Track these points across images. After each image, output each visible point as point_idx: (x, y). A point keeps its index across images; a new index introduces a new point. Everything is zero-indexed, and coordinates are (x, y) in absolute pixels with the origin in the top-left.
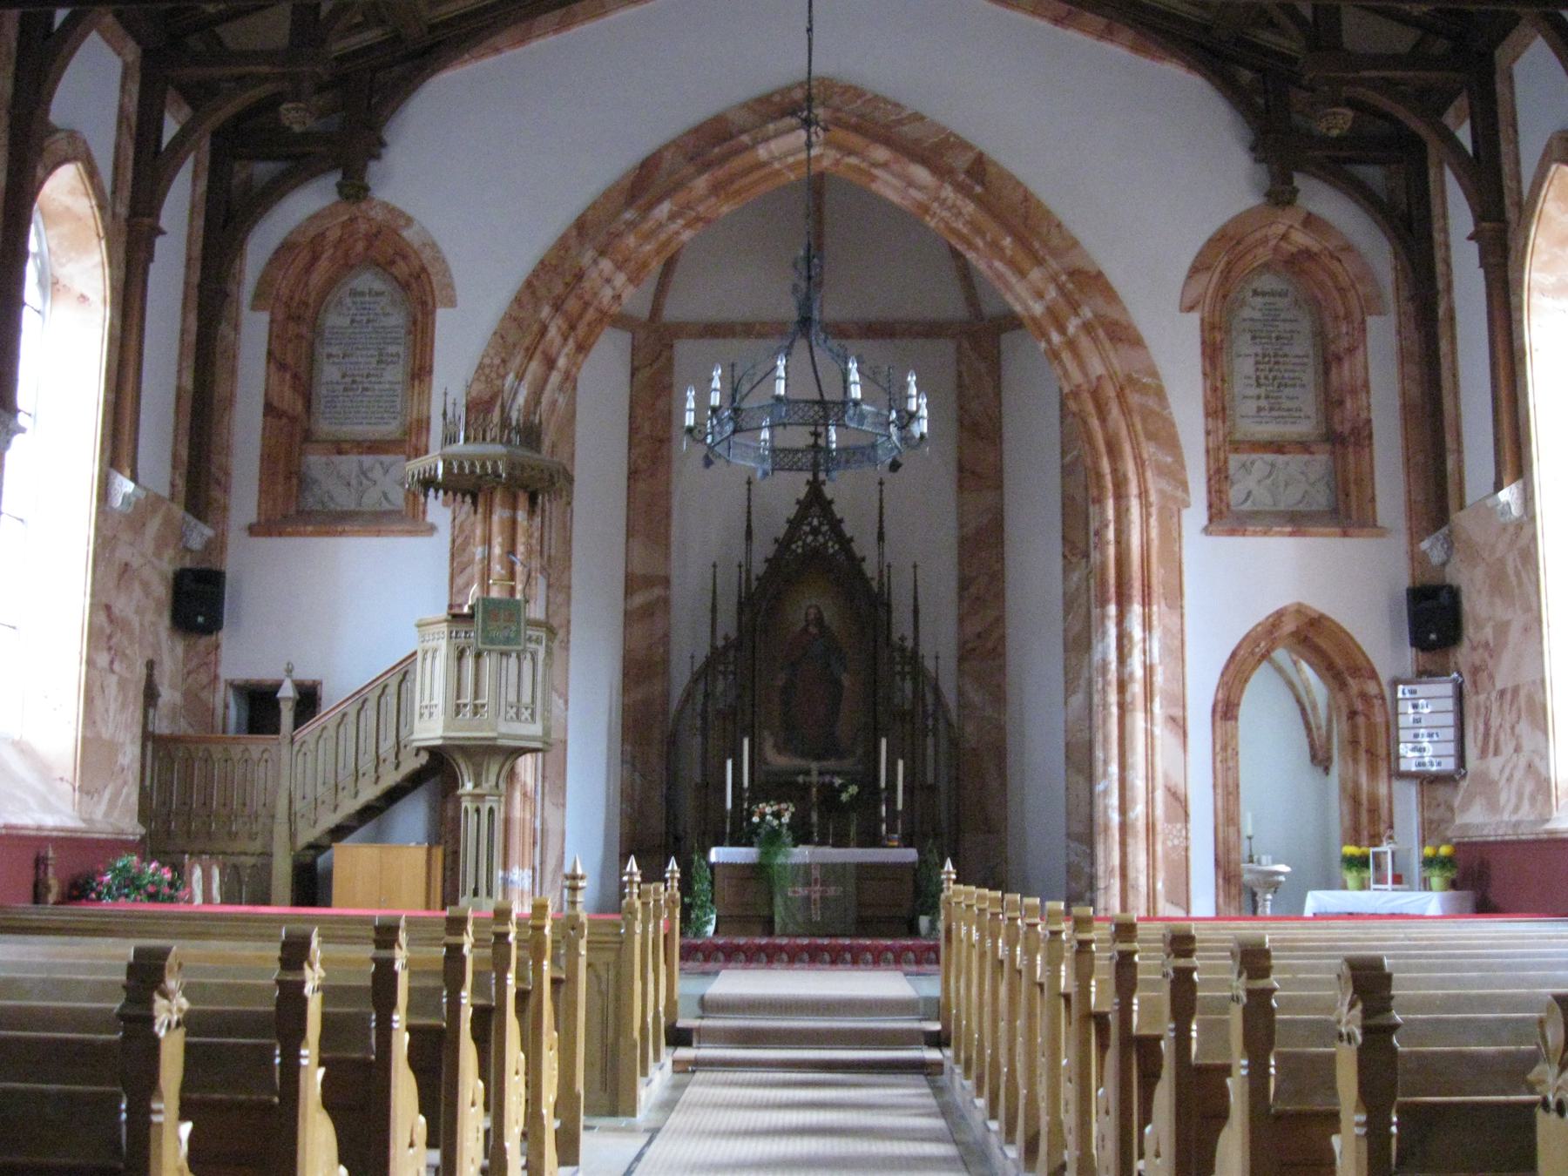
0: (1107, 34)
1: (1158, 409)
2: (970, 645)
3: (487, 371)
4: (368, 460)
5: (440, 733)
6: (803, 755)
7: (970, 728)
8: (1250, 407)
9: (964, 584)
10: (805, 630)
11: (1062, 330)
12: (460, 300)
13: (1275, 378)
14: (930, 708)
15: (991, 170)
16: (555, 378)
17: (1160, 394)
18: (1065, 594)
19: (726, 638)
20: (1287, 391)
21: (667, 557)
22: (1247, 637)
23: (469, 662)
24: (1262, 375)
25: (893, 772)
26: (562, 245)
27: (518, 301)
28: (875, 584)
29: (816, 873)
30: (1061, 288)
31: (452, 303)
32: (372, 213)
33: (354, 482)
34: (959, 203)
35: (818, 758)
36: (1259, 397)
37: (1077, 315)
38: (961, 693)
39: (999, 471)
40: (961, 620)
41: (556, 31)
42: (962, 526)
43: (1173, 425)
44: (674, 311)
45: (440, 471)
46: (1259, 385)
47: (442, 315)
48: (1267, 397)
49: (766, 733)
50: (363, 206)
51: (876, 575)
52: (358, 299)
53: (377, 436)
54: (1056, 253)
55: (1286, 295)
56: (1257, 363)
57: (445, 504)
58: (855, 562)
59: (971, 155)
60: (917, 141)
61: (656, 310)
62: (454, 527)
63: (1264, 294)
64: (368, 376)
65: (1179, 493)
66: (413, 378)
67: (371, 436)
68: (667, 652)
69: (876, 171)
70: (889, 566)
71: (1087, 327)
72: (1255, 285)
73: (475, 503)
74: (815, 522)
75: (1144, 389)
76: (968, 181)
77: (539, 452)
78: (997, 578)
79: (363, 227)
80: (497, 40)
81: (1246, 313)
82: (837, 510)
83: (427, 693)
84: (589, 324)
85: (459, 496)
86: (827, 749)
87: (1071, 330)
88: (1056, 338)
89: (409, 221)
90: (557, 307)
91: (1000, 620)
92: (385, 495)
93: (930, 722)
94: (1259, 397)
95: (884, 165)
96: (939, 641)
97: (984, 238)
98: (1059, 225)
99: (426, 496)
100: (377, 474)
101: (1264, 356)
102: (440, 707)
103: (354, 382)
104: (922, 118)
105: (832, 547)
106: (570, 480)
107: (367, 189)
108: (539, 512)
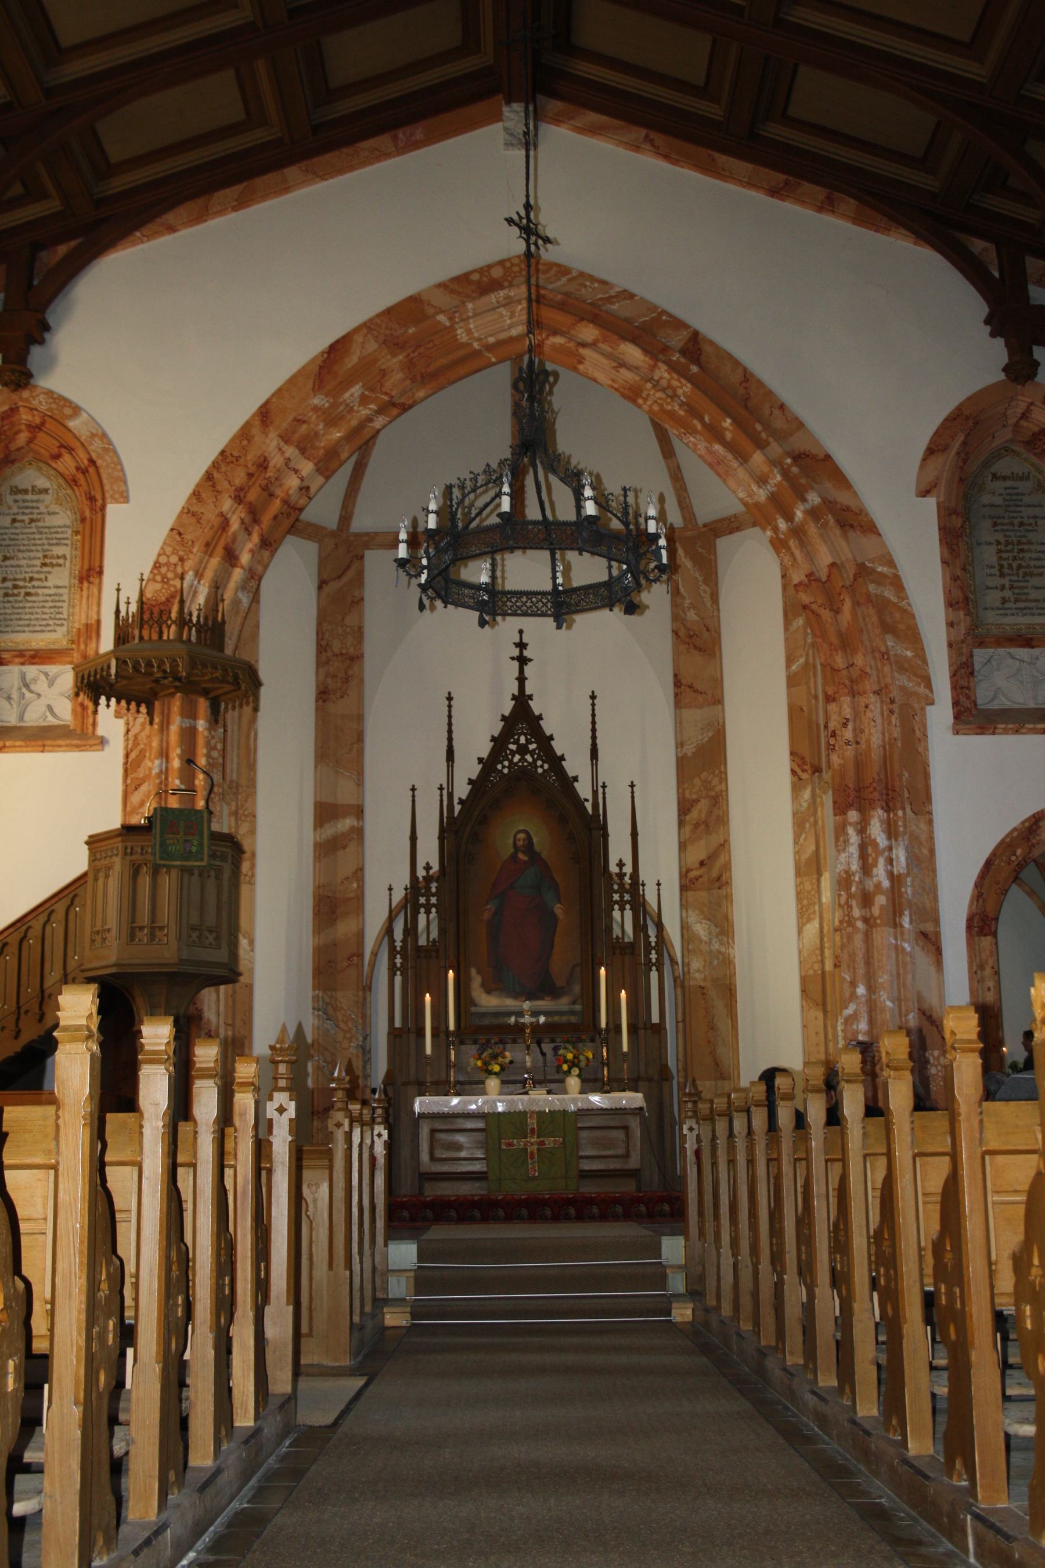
0: (826, 206)
1: (894, 599)
2: (692, 874)
3: (164, 570)
4: (32, 671)
5: (113, 959)
6: (516, 995)
7: (696, 964)
8: (993, 598)
9: (684, 808)
10: (514, 857)
11: (789, 517)
12: (131, 498)
13: (1020, 567)
14: (653, 940)
15: (707, 349)
16: (237, 574)
17: (897, 583)
18: (794, 814)
19: (428, 867)
20: (1034, 581)
21: (360, 783)
22: (1002, 842)
23: (145, 881)
24: (1005, 563)
25: (612, 1003)
26: (244, 434)
27: (196, 494)
28: (589, 806)
29: (532, 1123)
30: (785, 473)
31: (124, 497)
32: (35, 403)
33: (15, 695)
34: (675, 383)
35: (530, 997)
36: (1003, 588)
37: (804, 500)
38: (684, 927)
39: (718, 683)
40: (682, 846)
41: (235, 209)
42: (680, 745)
43: (913, 617)
44: (362, 522)
45: (113, 671)
46: (1002, 575)
47: (112, 510)
48: (1012, 588)
49: (473, 971)
50: (26, 394)
51: (590, 797)
52: (19, 497)
53: (42, 645)
54: (781, 436)
55: (1028, 478)
56: (999, 551)
57: (118, 715)
58: (568, 783)
59: (684, 335)
60: (628, 321)
61: (346, 518)
62: (127, 740)
63: (1004, 478)
64: (32, 579)
65: (922, 690)
66: (81, 581)
67: (34, 645)
68: (361, 888)
69: (583, 351)
70: (604, 787)
71: (813, 513)
72: (992, 470)
73: (150, 713)
74: (523, 740)
75: (880, 579)
76: (683, 360)
77: (221, 647)
78: (718, 800)
79: (25, 416)
80: (170, 217)
81: (986, 499)
82: (548, 727)
83: (99, 916)
84: (275, 518)
85: (133, 705)
86: (544, 987)
87: (799, 515)
88: (782, 525)
89: (77, 410)
90: (238, 499)
91: (724, 845)
92: (50, 708)
93: (653, 956)
94: (1003, 588)
95: (593, 345)
96: (661, 869)
97: (701, 420)
98: (782, 407)
99: (97, 704)
100: (41, 686)
101: (1007, 543)
102: (114, 932)
103: (15, 587)
104: (632, 296)
106: (256, 683)
107: (29, 375)
108: (221, 722)
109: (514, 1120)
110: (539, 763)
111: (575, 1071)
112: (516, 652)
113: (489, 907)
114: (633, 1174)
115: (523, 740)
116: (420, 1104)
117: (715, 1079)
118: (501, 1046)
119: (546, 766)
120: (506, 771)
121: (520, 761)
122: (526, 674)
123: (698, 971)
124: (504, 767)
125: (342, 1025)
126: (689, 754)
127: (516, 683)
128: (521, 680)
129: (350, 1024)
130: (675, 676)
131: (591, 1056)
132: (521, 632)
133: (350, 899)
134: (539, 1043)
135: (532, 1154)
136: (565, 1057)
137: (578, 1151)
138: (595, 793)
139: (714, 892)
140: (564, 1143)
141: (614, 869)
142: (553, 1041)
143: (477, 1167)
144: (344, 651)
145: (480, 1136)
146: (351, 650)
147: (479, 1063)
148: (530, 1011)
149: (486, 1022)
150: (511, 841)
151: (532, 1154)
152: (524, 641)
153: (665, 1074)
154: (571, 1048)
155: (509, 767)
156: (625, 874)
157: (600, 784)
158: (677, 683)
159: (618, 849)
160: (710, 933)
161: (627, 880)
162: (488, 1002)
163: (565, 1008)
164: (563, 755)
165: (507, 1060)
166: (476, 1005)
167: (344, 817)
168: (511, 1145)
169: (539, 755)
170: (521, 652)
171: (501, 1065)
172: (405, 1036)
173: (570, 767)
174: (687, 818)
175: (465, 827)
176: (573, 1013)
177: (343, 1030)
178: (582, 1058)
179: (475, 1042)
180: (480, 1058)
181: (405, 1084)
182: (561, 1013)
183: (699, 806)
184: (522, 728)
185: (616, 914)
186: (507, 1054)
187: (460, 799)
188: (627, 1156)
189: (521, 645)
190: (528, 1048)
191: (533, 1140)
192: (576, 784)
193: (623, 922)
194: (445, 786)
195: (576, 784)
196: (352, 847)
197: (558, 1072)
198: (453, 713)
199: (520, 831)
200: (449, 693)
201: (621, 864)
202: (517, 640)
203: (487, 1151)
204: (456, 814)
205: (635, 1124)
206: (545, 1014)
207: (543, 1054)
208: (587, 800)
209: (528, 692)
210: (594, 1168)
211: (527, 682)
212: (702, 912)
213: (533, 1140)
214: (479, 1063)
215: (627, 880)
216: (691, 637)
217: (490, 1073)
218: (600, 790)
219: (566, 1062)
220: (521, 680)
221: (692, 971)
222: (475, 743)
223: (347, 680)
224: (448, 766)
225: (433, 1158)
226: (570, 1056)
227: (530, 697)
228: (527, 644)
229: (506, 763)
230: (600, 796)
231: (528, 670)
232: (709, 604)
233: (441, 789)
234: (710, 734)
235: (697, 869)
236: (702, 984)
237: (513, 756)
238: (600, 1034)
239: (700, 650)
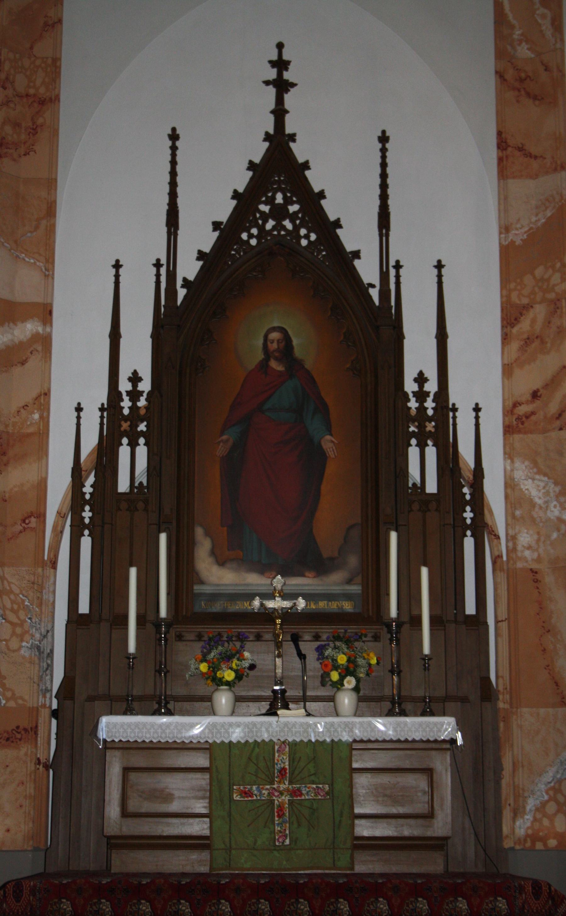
2: (522, 410)
6: (262, 569)
7: (525, 538)
9: (511, 316)
10: (264, 365)
19: (135, 379)
21: (48, 273)
25: (406, 585)
28: (374, 294)
29: (283, 761)
38: (510, 485)
40: (508, 371)
42: (505, 229)
51: (376, 281)
58: (346, 260)
70: (398, 266)
74: (279, 199)
82: (316, 179)
86: (306, 558)
105: (307, 238)
109: (255, 757)
110: (303, 232)
111: (350, 682)
112: (272, 74)
113: (224, 437)
114: (438, 844)
115: (279, 199)
116: (112, 726)
117: (554, 706)
118: (238, 644)
119: (313, 237)
120: (253, 242)
121: (274, 228)
122: (287, 106)
123: (529, 548)
124: (251, 236)
125: (12, 617)
126: (518, 242)
127: (272, 118)
128: (280, 113)
129: (22, 614)
130: (499, 133)
131: (374, 661)
132: (280, 46)
133: (29, 435)
134: (296, 639)
135: (281, 808)
136: (334, 660)
137: (352, 808)
138: (384, 276)
139: (554, 434)
140: (331, 793)
141: (410, 386)
142: (317, 637)
143: (198, 828)
144: (32, 91)
145: (202, 780)
146: (42, 90)
147: (204, 667)
148: (279, 593)
149: (217, 607)
150: (261, 342)
151: (281, 808)
152: (285, 57)
153: (487, 692)
154: (344, 646)
155: (258, 237)
156: (428, 394)
157: (392, 263)
158: (502, 144)
159: (418, 356)
160: (547, 493)
161: (430, 404)
162: (218, 577)
163: (337, 589)
164: (338, 220)
165: (246, 664)
166: (202, 582)
167: (24, 320)
168: (248, 794)
169: (302, 219)
170: (280, 74)
171: (236, 671)
172: (93, 629)
173: (349, 239)
174: (515, 330)
175: (189, 323)
176: (348, 597)
177: (11, 623)
178: (360, 661)
179: (199, 637)
180: (204, 660)
181: (91, 699)
182: (329, 597)
183: (531, 314)
184: (279, 182)
185: (413, 452)
186: (246, 654)
187: (185, 279)
188: (430, 816)
189: (281, 64)
190: (279, 645)
191: (282, 787)
192: (356, 263)
193: (422, 467)
194: (164, 261)
195: (356, 263)
196: (34, 362)
197: (323, 684)
198: (178, 159)
199: (274, 329)
200: (174, 129)
201: (421, 379)
202: (275, 57)
203: (210, 803)
204: (179, 303)
205: (442, 765)
206: (306, 597)
207: (302, 656)
208: (373, 286)
209: (289, 130)
210: (378, 833)
211: (288, 117)
212: (535, 463)
213: (282, 787)
214: (204, 667)
215: (430, 404)
216: (522, 80)
217: (219, 682)
218: (392, 272)
219: (336, 667)
220: (280, 113)
221: (519, 548)
222: (208, 206)
223: (34, 130)
224: (169, 234)
225: (125, 813)
226: (342, 659)
227: (292, 137)
228: (288, 63)
229: (254, 231)
230: (392, 280)
231: (289, 99)
232: (549, 33)
233: (158, 265)
234: (549, 214)
235: (527, 402)
236: (535, 566)
237: (265, 222)
238: (389, 626)
239: (535, 98)
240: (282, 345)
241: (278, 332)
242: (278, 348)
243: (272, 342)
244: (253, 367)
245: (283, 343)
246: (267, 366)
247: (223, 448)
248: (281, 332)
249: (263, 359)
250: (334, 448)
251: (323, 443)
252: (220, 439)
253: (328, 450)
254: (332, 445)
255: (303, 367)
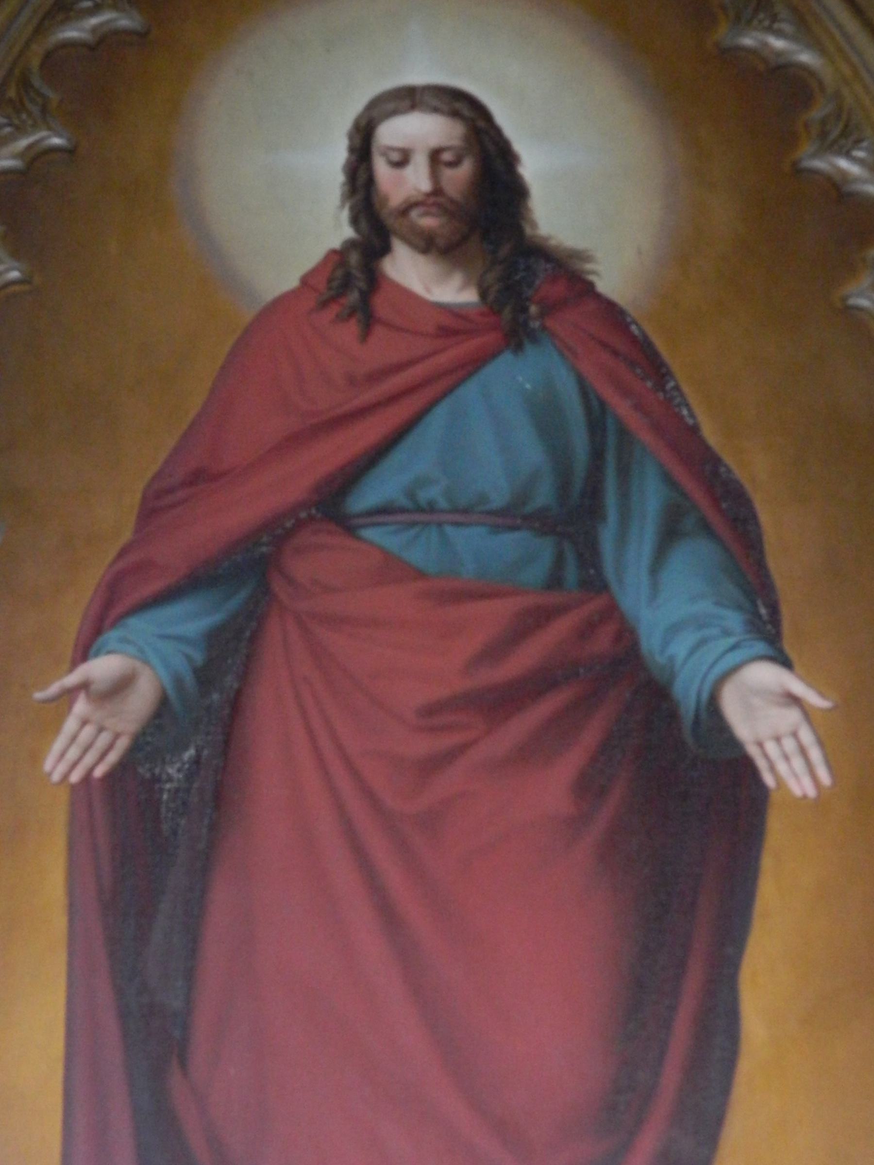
10: (353, 279)
113: (103, 667)
150: (337, 154)
199: (409, 98)
240: (459, 177)
241: (436, 110)
242: (437, 191)
243: (403, 160)
244: (291, 282)
245: (466, 168)
246: (374, 279)
247: (88, 732)
248: (455, 114)
249: (350, 245)
250: (807, 736)
251: (732, 707)
252: (72, 679)
253: (771, 748)
254: (793, 715)
255: (588, 290)
